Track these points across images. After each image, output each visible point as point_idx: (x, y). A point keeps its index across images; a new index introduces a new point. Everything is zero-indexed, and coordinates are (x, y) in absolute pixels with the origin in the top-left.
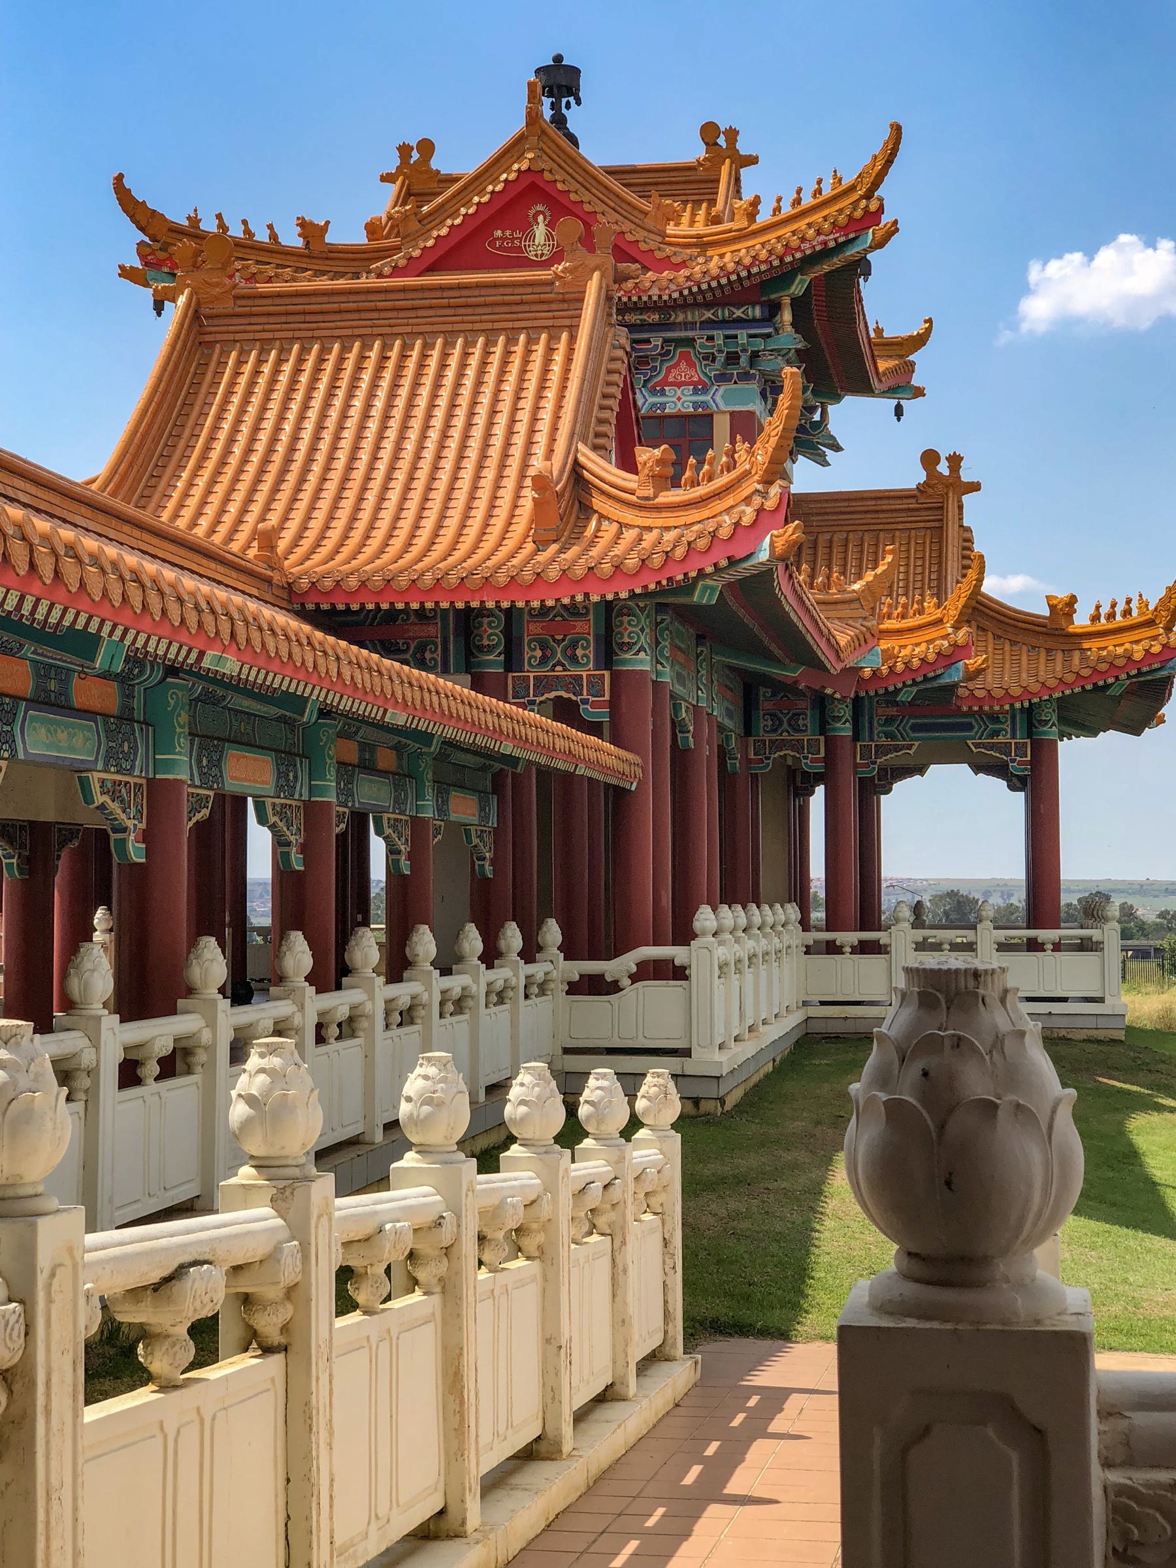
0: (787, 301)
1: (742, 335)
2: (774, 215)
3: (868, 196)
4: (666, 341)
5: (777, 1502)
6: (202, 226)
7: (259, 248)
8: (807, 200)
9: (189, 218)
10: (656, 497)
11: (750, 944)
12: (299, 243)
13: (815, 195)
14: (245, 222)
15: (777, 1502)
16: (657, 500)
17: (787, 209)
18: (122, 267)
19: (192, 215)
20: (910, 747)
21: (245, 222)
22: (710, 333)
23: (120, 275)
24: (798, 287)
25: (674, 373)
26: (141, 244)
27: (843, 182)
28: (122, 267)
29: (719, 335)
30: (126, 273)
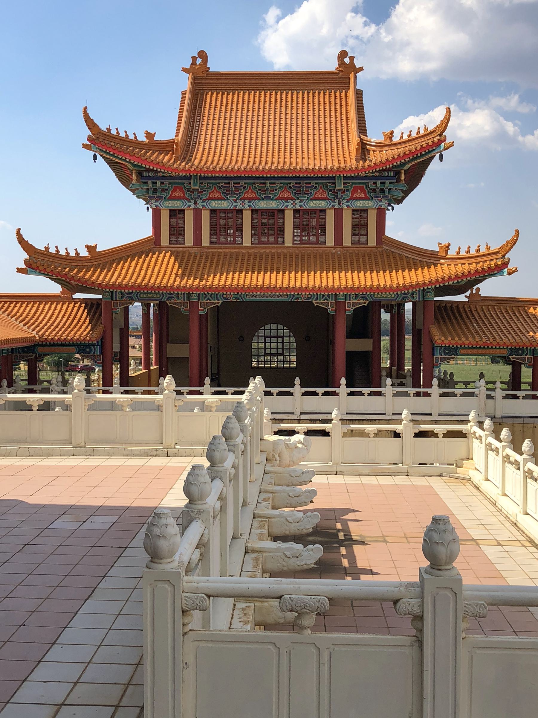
0: (403, 171)
1: (387, 182)
2: (401, 139)
3: (440, 135)
4: (245, 183)
5: (362, 521)
6: (112, 132)
7: (131, 141)
8: (414, 135)
9: (107, 129)
10: (446, 256)
11: (194, 272)
12: (145, 140)
13: (418, 133)
14: (126, 132)
15: (362, 521)
16: (447, 257)
17: (405, 137)
18: (18, 269)
19: (108, 128)
20: (365, 303)
21: (126, 132)
22: (375, 181)
23: (83, 147)
24: (407, 167)
25: (356, 194)
26: (89, 137)
27: (428, 130)
28: (18, 269)
29: (379, 182)
30: (85, 146)
